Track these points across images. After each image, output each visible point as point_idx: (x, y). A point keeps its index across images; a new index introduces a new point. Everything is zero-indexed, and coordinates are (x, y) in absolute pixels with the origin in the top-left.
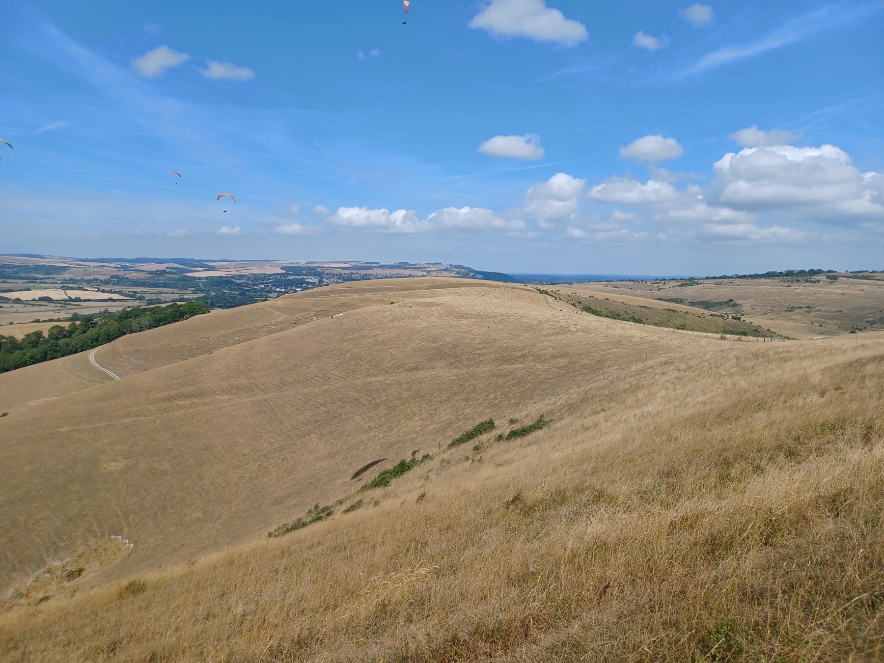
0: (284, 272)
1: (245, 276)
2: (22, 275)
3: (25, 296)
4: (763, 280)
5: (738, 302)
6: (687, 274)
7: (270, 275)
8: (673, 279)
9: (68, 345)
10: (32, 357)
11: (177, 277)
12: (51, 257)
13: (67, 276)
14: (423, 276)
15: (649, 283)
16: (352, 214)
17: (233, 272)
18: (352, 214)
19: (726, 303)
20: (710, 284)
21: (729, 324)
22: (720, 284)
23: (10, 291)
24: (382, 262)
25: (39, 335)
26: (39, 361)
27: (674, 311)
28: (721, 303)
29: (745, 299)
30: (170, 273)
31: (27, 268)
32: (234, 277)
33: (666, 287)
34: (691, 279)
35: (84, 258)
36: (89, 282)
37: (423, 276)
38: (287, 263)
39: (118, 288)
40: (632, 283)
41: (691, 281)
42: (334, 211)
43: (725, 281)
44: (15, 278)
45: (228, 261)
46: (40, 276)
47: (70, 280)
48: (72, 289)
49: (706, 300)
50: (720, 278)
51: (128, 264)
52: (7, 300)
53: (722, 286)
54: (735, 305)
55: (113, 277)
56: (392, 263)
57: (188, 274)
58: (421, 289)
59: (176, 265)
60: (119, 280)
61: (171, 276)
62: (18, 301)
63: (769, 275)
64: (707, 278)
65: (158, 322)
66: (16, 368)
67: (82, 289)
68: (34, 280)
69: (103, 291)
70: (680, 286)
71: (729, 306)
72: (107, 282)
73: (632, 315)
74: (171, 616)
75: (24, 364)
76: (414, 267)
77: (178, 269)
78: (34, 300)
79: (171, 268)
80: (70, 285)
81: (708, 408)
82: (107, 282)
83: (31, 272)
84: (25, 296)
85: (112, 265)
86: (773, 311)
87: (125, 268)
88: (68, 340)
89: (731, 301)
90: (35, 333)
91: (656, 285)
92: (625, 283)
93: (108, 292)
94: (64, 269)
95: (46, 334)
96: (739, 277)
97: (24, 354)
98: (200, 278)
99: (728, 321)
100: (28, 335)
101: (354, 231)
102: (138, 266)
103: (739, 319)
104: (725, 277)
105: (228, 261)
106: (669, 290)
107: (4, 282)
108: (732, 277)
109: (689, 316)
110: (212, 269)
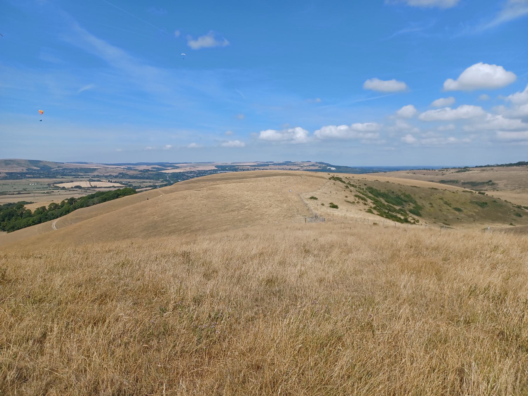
0: (216, 168)
1: (193, 172)
2: (73, 174)
3: (67, 185)
4: (515, 167)
5: (496, 182)
6: (463, 165)
7: (208, 171)
8: (454, 168)
9: (53, 215)
10: (33, 222)
11: (155, 173)
12: (92, 163)
13: (96, 173)
14: (298, 169)
15: (437, 171)
16: (268, 134)
17: (188, 169)
18: (268, 134)
19: (487, 183)
20: (476, 171)
21: (475, 197)
22: (484, 170)
23: (62, 183)
24: (276, 162)
25: (44, 208)
26: (37, 224)
27: (436, 189)
28: (483, 183)
29: (500, 180)
30: (152, 171)
31: (76, 170)
32: (187, 172)
33: (448, 173)
34: (466, 168)
35: (109, 163)
36: (106, 177)
37: (298, 169)
38: (220, 164)
39: (121, 180)
40: (425, 171)
41: (466, 169)
42: (259, 134)
43: (488, 168)
44: (68, 176)
45: (186, 163)
46: (82, 174)
47: (97, 176)
48: (94, 181)
49: (474, 180)
50: (485, 166)
51: (132, 166)
52: (58, 188)
53: (485, 172)
54: (493, 184)
55: (120, 174)
56: (282, 162)
57: (163, 171)
58: (250, 178)
59: (157, 166)
60: (123, 175)
61: (152, 172)
62: (64, 188)
63: (520, 164)
64: (477, 167)
65: (105, 200)
66: (25, 227)
67: (100, 181)
68: (77, 176)
69: (111, 182)
70: (457, 172)
71: (489, 185)
72: (116, 177)
73: (404, 192)
74: (406, 331)
75: (30, 225)
76: (294, 164)
77: (158, 168)
78: (72, 188)
79: (154, 168)
80: (94, 179)
81: (194, 283)
82: (116, 177)
83: (78, 172)
84: (67, 185)
85: (122, 167)
86: (520, 188)
87: (129, 169)
88: (53, 211)
89: (490, 181)
90: (41, 208)
91: (441, 172)
92: (420, 171)
93: (114, 182)
94: (95, 169)
95: (47, 208)
96: (498, 166)
97: (29, 220)
98: (168, 173)
99: (475, 195)
100: (38, 209)
101: (268, 143)
102: (137, 167)
103: (483, 194)
104: (488, 166)
105: (186, 163)
106: (449, 175)
107: (62, 178)
108: (493, 166)
109: (447, 192)
110: (178, 168)
